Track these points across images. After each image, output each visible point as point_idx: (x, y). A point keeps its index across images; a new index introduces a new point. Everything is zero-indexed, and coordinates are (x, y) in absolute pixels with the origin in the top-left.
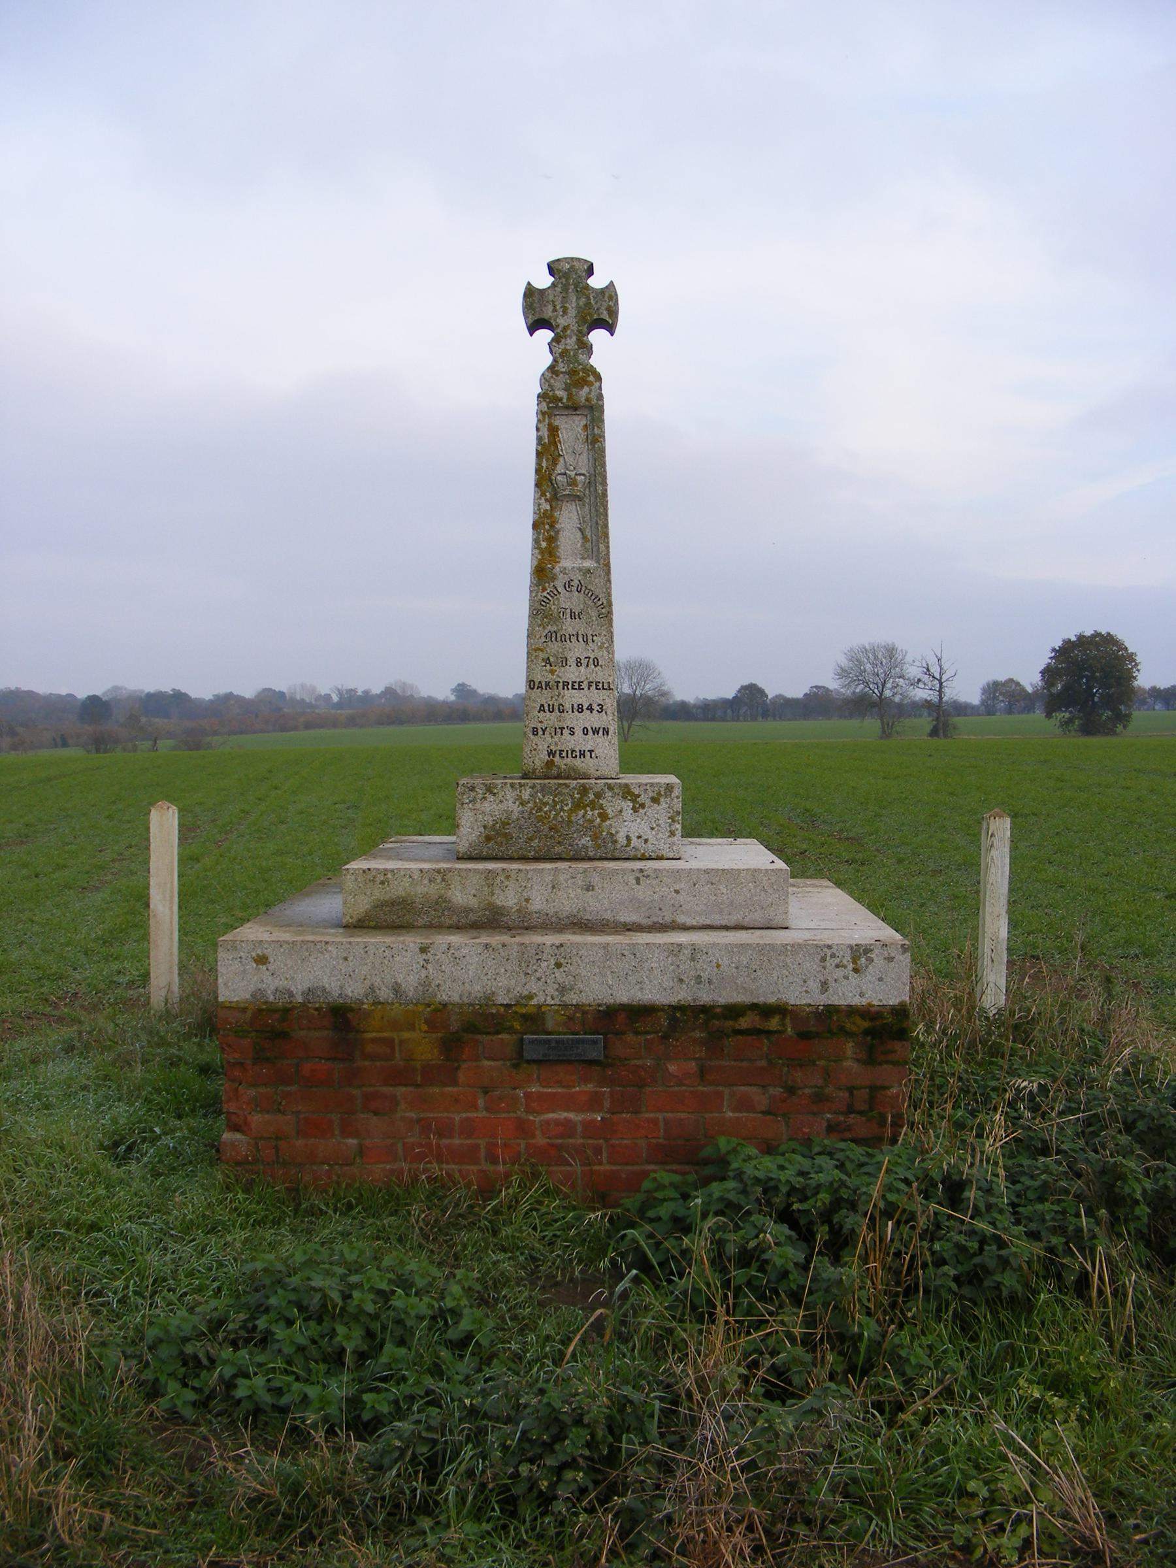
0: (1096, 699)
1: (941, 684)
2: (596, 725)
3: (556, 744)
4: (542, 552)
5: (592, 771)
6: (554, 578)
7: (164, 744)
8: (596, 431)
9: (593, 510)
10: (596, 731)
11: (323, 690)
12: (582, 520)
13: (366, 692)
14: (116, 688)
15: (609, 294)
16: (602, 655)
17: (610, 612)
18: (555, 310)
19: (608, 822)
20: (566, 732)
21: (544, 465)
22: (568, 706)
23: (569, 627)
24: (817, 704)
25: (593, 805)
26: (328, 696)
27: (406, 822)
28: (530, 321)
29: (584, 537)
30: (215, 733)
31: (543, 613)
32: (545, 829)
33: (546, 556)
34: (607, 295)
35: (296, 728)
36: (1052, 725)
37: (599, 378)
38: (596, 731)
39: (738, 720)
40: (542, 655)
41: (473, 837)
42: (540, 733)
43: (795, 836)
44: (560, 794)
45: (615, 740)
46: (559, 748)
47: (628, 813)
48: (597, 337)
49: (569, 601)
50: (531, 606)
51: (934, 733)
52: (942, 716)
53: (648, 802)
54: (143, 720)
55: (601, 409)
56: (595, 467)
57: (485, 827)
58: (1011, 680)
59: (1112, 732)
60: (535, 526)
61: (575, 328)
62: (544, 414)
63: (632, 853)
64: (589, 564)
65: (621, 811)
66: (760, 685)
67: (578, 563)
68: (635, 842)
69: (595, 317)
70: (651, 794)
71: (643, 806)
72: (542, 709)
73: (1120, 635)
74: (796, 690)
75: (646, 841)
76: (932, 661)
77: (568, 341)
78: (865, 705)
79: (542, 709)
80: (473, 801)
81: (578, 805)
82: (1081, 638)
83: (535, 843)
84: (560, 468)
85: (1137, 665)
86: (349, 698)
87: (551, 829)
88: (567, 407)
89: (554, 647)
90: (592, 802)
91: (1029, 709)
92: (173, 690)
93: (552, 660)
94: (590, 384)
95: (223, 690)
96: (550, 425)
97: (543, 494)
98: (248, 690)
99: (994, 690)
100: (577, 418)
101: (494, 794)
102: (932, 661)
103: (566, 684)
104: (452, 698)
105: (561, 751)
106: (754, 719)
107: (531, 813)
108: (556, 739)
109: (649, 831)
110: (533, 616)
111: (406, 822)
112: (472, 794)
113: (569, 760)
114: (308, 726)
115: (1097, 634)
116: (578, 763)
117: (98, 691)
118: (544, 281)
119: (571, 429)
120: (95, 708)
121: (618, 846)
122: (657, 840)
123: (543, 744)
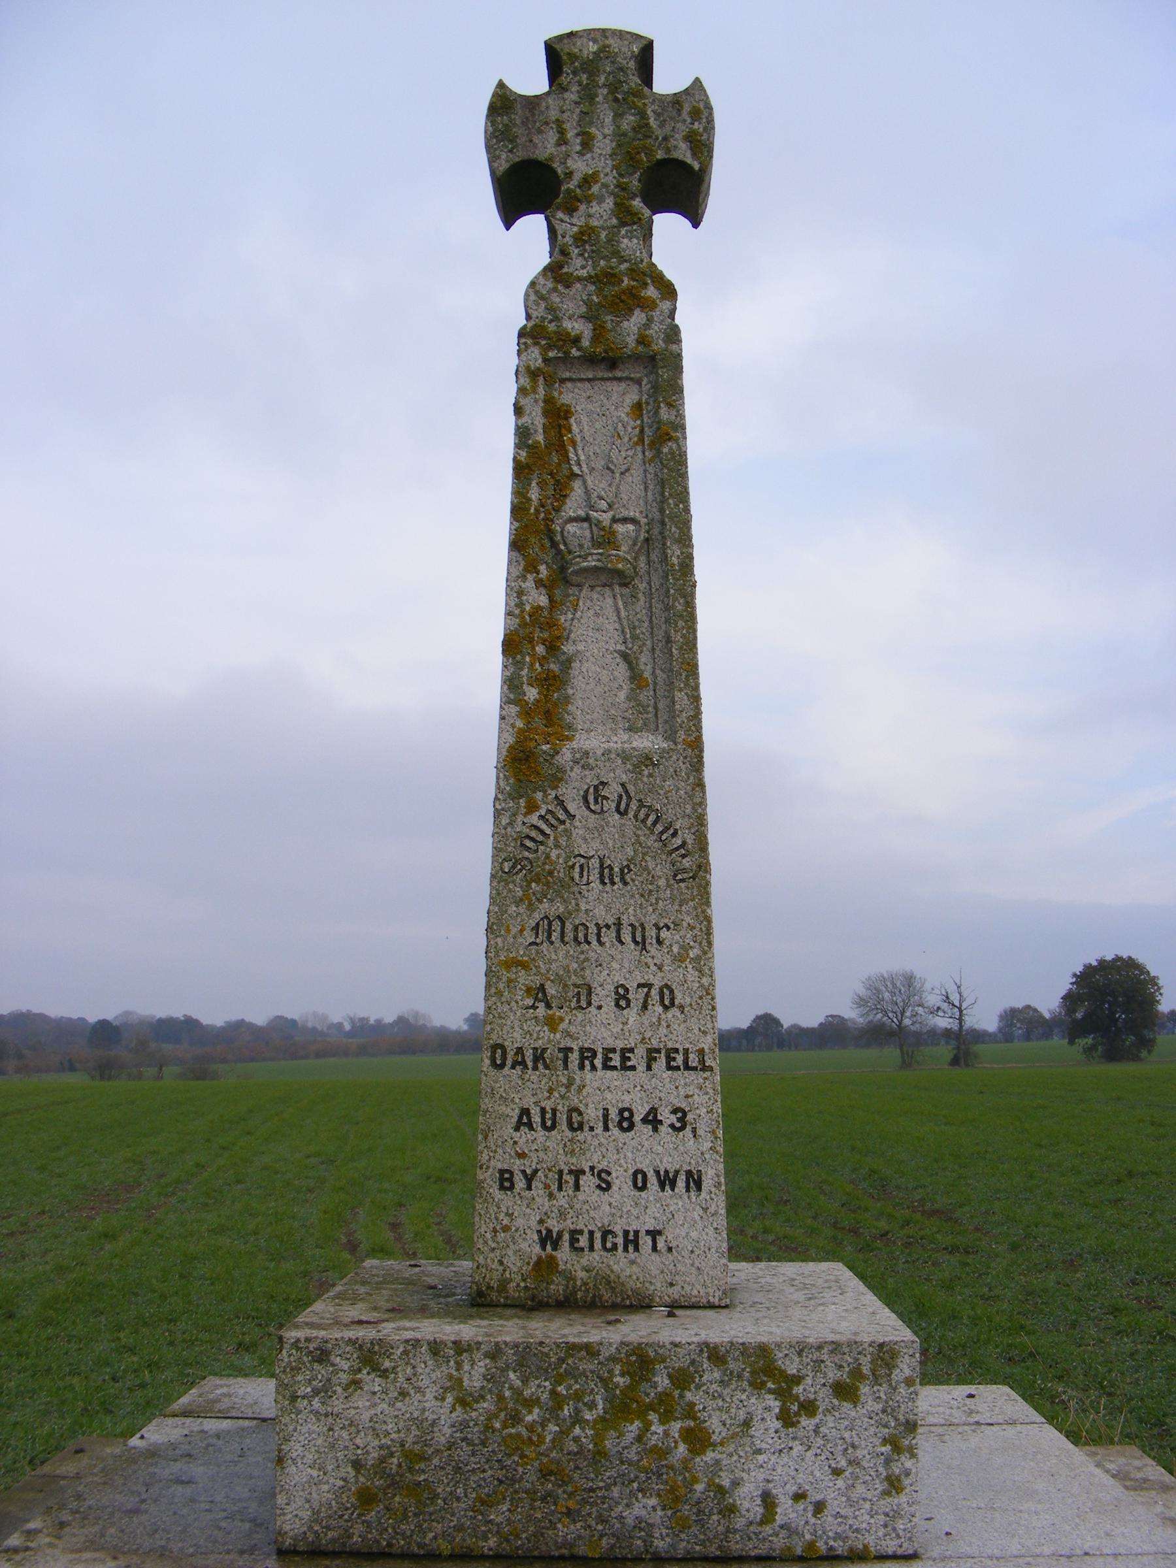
0: (1119, 1024)
1: (961, 1011)
2: (668, 1164)
3: (562, 1215)
4: (527, 712)
5: (658, 1287)
6: (557, 778)
7: (170, 1071)
8: (665, 414)
9: (657, 607)
10: (667, 1180)
11: (336, 1018)
12: (629, 633)
13: (379, 1021)
14: (127, 1013)
15: (694, 106)
16: (683, 979)
17: (703, 867)
18: (562, 141)
19: (710, 1456)
20: (588, 1181)
21: (534, 494)
22: (592, 1114)
23: (597, 903)
24: (832, 1033)
25: (666, 1407)
26: (340, 1025)
27: (386, 1185)
28: (503, 166)
29: (636, 677)
30: (224, 1061)
31: (526, 869)
32: (530, 1477)
33: (538, 722)
34: (687, 108)
35: (306, 1057)
36: (1076, 1051)
37: (669, 292)
38: (667, 1180)
39: (753, 1050)
40: (524, 978)
41: (323, 1494)
42: (520, 1184)
43: (866, 1210)
44: (571, 1374)
45: (719, 1204)
46: (569, 1224)
47: (767, 1428)
48: (668, 227)
49: (596, 837)
50: (497, 850)
51: (955, 1062)
52: (963, 1045)
53: (824, 1398)
54: (153, 1046)
55: (675, 363)
56: (663, 501)
57: (357, 1465)
58: (1028, 1007)
59: (1137, 1058)
60: (510, 646)
61: (610, 179)
62: (533, 374)
63: (779, 1543)
64: (647, 742)
65: (747, 1424)
66: (776, 1014)
67: (621, 740)
68: (786, 1511)
69: (660, 155)
70: (832, 1375)
71: (809, 1408)
72: (524, 1120)
73: (1141, 958)
74: (811, 1019)
75: (819, 1507)
76: (952, 988)
77: (595, 208)
78: (877, 1034)
79: (524, 1120)
80: (324, 1391)
81: (623, 1408)
82: (1102, 962)
83: (499, 1514)
84: (573, 506)
85: (1159, 988)
86: (362, 1028)
87: (545, 1474)
88: (590, 360)
89: (558, 957)
90: (664, 1399)
91: (1047, 1035)
92: (185, 1016)
93: (551, 990)
94: (648, 305)
95: (234, 1017)
96: (549, 401)
97: (531, 567)
98: (259, 1017)
99: (1011, 1017)
100: (616, 388)
101: (384, 1374)
102: (952, 988)
103: (587, 1055)
104: (465, 1028)
105: (575, 1234)
106: (769, 1048)
107: (488, 1428)
108: (562, 1200)
109: (828, 1479)
110: (500, 877)
111: (386, 1185)
112: (322, 1371)
113: (596, 1257)
114: (319, 1055)
115: (1118, 959)
116: (620, 1264)
117: (109, 1015)
118: (532, 80)
119: (600, 413)
120: (105, 1032)
121: (740, 1523)
122: (851, 1503)
123: (527, 1213)
